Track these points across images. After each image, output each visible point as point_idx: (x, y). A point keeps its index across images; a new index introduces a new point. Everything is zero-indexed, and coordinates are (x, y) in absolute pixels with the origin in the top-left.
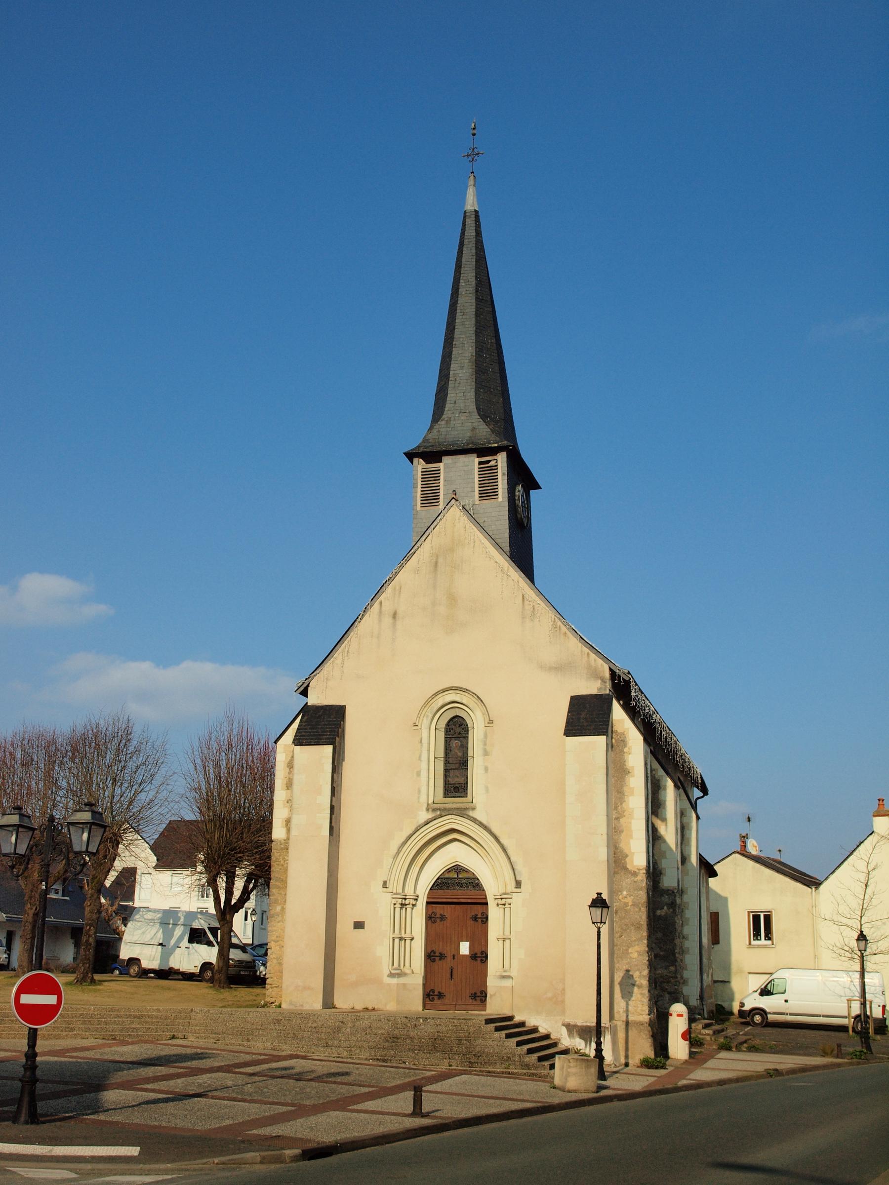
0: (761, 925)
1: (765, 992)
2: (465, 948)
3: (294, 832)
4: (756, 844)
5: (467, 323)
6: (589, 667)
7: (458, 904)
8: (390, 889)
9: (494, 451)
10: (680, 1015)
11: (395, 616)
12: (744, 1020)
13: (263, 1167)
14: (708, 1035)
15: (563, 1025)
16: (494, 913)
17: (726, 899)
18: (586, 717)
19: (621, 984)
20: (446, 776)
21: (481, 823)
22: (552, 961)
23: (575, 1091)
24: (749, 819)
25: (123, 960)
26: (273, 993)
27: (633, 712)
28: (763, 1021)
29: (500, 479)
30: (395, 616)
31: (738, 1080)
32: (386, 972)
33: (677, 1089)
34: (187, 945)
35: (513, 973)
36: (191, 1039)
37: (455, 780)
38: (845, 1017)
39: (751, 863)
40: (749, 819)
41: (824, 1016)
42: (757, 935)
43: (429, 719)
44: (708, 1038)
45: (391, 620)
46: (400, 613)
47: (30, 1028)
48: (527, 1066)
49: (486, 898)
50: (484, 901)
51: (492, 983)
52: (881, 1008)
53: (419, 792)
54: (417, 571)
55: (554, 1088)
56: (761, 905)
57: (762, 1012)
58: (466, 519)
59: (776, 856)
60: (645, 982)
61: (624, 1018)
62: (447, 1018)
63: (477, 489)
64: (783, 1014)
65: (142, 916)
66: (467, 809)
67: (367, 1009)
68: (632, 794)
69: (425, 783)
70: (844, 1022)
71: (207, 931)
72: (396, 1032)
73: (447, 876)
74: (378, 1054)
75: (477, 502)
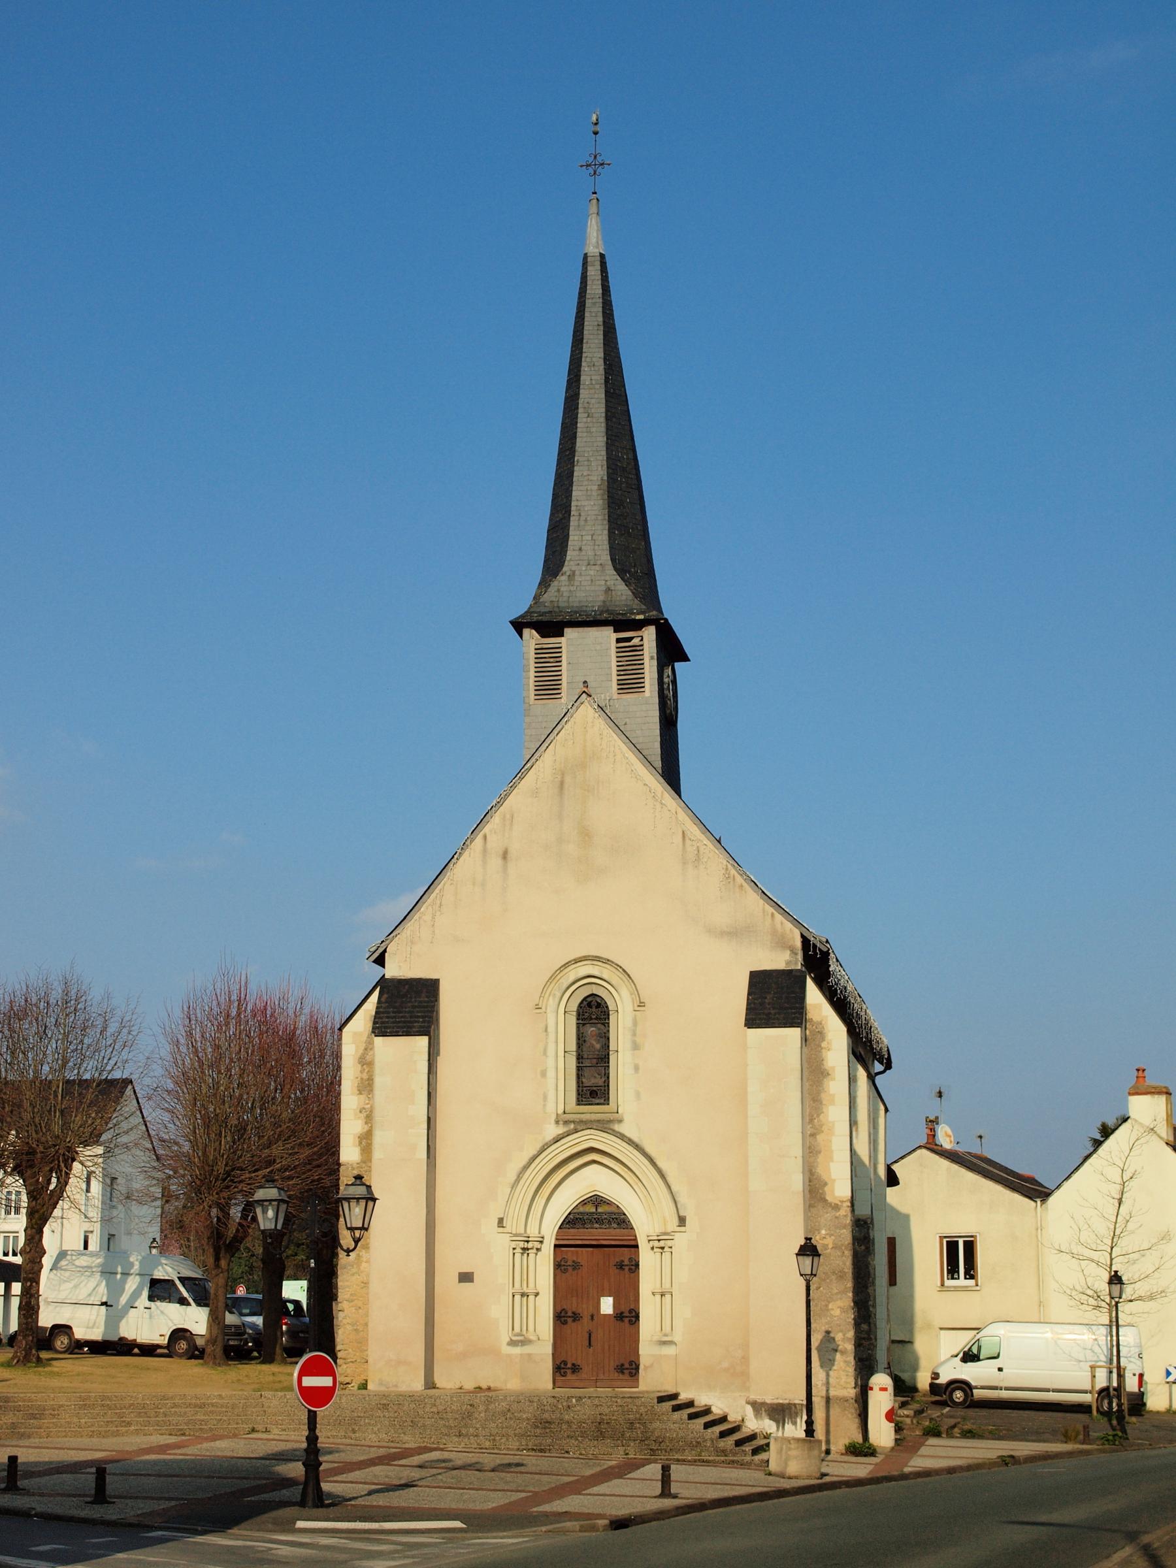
0: (960, 1257)
1: (970, 1357)
2: (607, 1305)
3: (377, 1154)
4: (949, 1132)
5: (594, 430)
6: (774, 932)
7: (597, 1249)
8: (508, 1229)
9: (639, 625)
10: (884, 1389)
11: (505, 855)
12: (938, 1398)
13: (581, 1534)
14: (908, 1416)
15: (748, 1403)
16: (647, 1258)
17: (906, 1218)
18: (772, 1000)
19: (819, 1349)
20: (578, 1077)
21: (630, 1140)
22: (726, 1322)
23: (796, 1477)
24: (940, 1094)
25: (45, 1329)
26: (349, 1371)
27: (841, 1005)
28: (965, 1400)
29: (647, 666)
30: (505, 855)
31: (969, 1468)
32: (505, 1337)
33: (904, 1477)
34: (148, 1304)
35: (677, 1337)
36: (276, 1431)
37: (592, 1080)
38: (1085, 1392)
39: (945, 1163)
40: (940, 1094)
41: (1054, 1391)
42: (953, 1271)
43: (557, 1000)
44: (908, 1421)
45: (500, 861)
46: (513, 853)
47: (309, 1411)
48: (724, 1452)
49: (636, 1239)
50: (633, 1243)
51: (646, 1350)
52: (1136, 1378)
53: (545, 1098)
54: (535, 793)
55: (770, 1474)
56: (960, 1228)
57: (964, 1385)
58: (603, 722)
59: (976, 1150)
60: (850, 1347)
61: (824, 1393)
62: (596, 1398)
63: (615, 678)
64: (995, 1388)
65: (72, 1262)
66: (610, 1121)
67: (480, 1388)
68: (832, 1102)
69: (554, 1087)
70: (1087, 1398)
71: (178, 1282)
72: (546, 1416)
73: (581, 1209)
74: (530, 1444)
75: (615, 696)
